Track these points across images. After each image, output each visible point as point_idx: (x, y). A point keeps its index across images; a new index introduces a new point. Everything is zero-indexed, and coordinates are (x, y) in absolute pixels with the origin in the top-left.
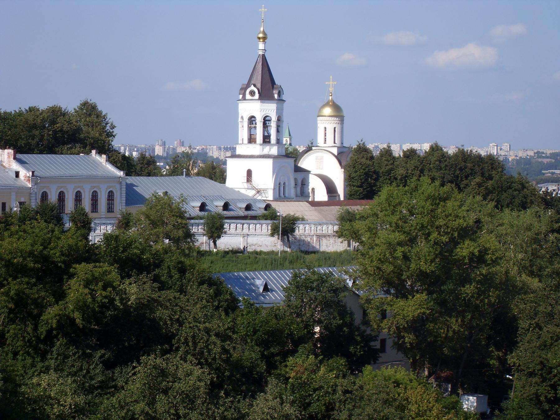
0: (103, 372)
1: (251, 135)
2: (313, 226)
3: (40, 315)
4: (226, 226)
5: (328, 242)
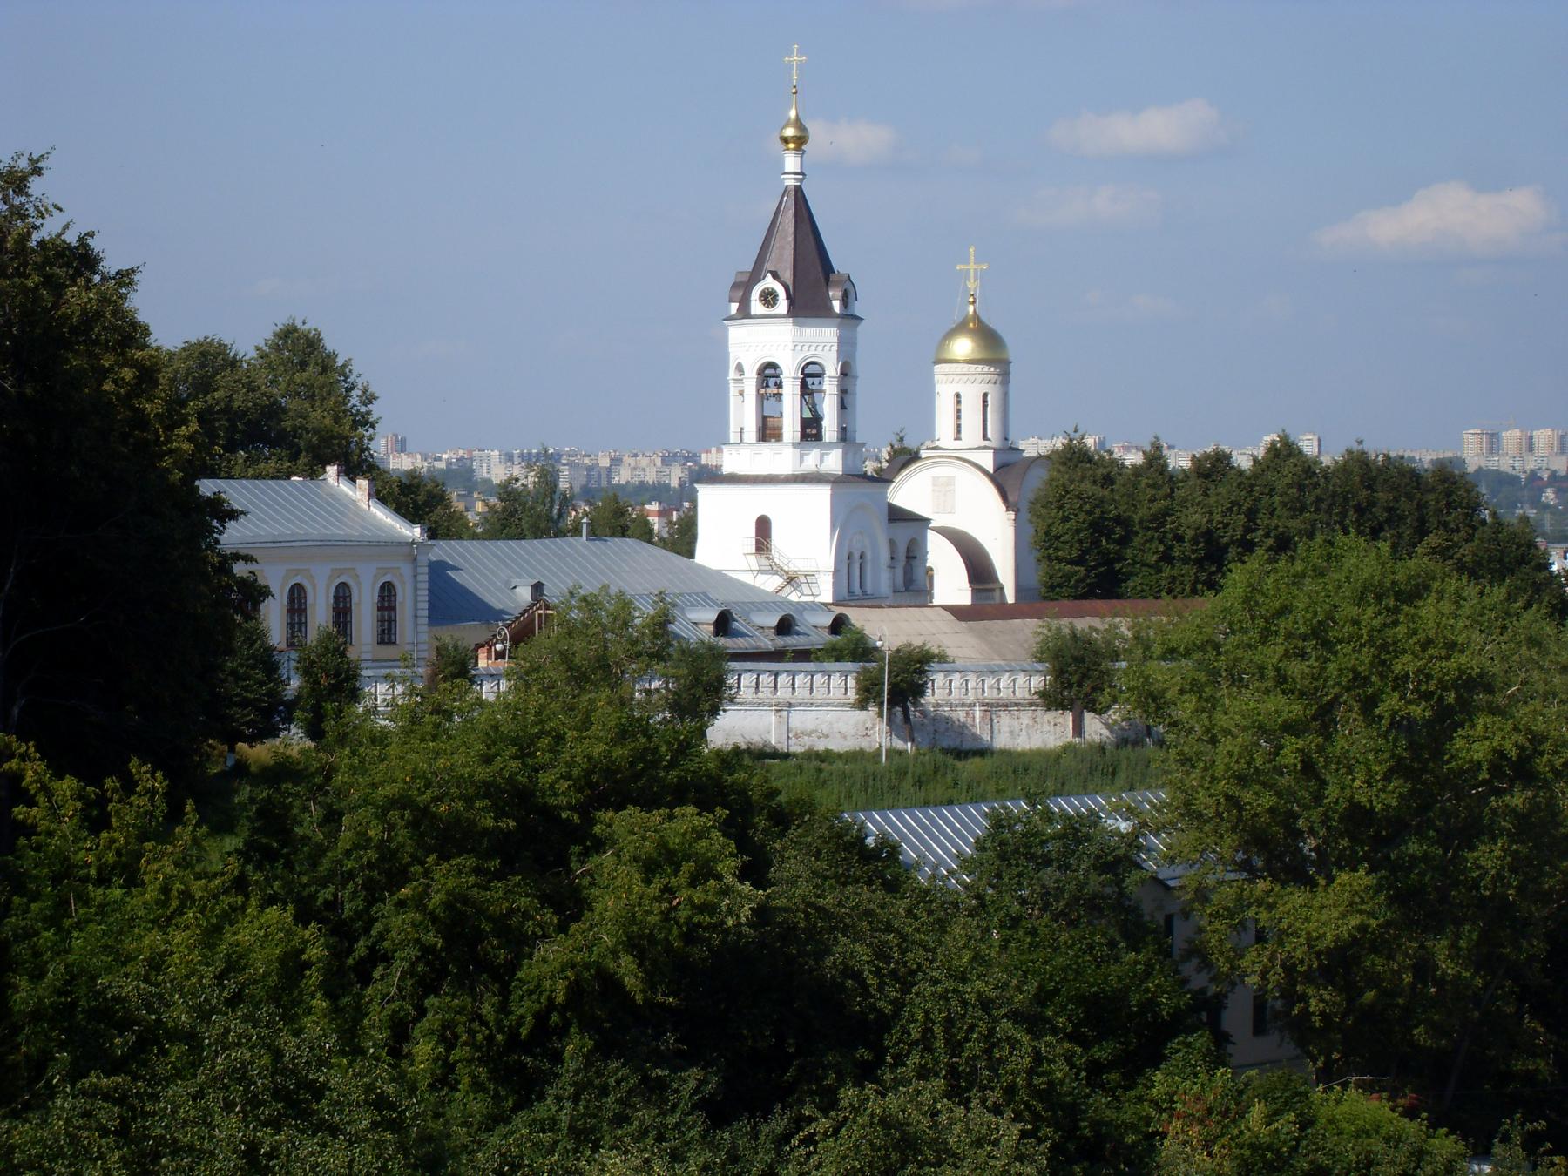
0: (704, 1137)
1: (765, 418)
2: (972, 678)
3: (513, 966)
4: (732, 681)
5: (1016, 723)
